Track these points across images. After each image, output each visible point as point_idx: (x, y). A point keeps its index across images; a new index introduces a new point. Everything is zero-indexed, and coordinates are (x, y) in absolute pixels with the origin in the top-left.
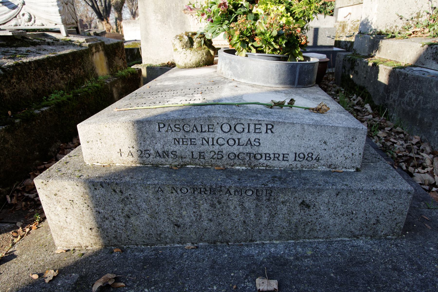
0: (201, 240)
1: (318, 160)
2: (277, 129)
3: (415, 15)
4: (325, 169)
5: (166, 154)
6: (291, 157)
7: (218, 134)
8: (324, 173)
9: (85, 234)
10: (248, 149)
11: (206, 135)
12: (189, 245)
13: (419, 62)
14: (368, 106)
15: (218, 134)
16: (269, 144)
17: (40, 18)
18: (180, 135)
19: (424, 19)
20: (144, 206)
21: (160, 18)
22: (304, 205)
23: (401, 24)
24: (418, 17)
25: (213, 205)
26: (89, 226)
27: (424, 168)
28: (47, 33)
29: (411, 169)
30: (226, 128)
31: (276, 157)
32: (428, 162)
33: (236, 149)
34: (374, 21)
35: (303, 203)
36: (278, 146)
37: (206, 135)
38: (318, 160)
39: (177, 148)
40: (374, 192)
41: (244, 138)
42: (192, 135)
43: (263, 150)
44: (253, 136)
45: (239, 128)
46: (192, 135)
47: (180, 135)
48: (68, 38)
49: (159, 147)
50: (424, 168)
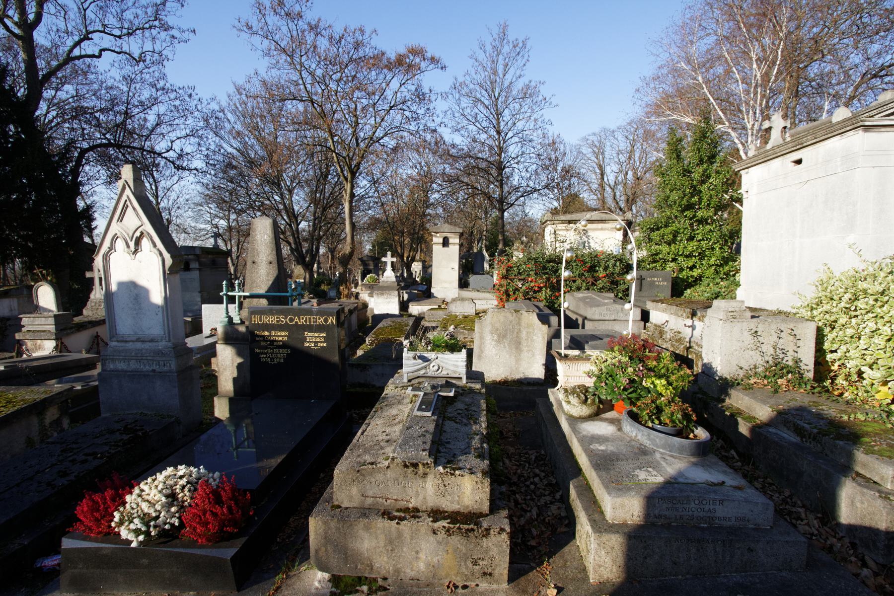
0: (688, 574)
1: (748, 521)
2: (726, 503)
3: (752, 367)
4: (752, 526)
5: (660, 516)
6: (733, 519)
7: (692, 505)
8: (754, 529)
9: (614, 570)
10: (709, 514)
11: (685, 506)
12: (680, 577)
13: (770, 423)
14: (733, 452)
15: (692, 505)
16: (721, 511)
17: (447, 369)
18: (670, 505)
19: (760, 370)
20: (657, 550)
21: (495, 338)
22: (750, 550)
23: (742, 373)
24: (755, 367)
25: (698, 550)
26: (618, 564)
27: (802, 520)
28: (454, 382)
29: (794, 521)
30: (697, 502)
31: (725, 519)
32: (803, 516)
33: (701, 514)
34: (719, 369)
35: (749, 548)
36: (725, 512)
37: (685, 506)
38: (748, 521)
39: (667, 513)
40: (787, 542)
41: (707, 508)
42: (677, 506)
43: (717, 515)
44: (712, 507)
45: (704, 502)
46: (677, 506)
47: (670, 505)
48: (470, 385)
49: (657, 512)
50: (802, 520)
